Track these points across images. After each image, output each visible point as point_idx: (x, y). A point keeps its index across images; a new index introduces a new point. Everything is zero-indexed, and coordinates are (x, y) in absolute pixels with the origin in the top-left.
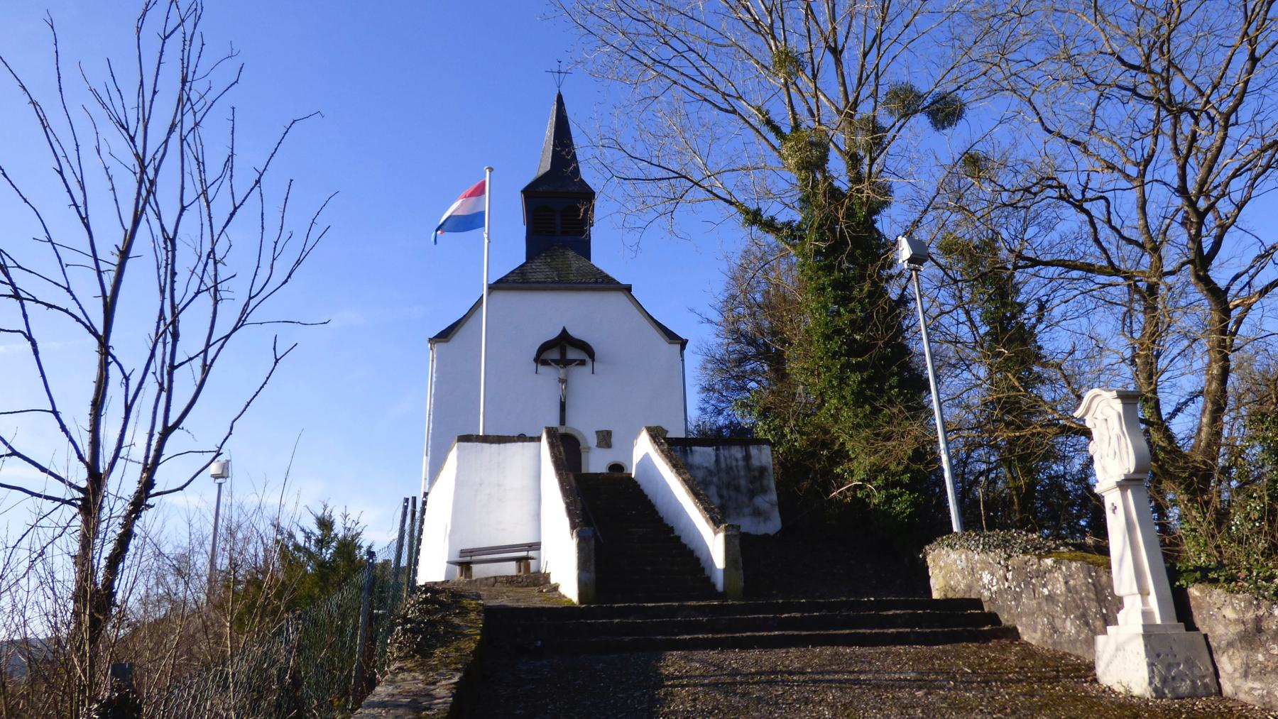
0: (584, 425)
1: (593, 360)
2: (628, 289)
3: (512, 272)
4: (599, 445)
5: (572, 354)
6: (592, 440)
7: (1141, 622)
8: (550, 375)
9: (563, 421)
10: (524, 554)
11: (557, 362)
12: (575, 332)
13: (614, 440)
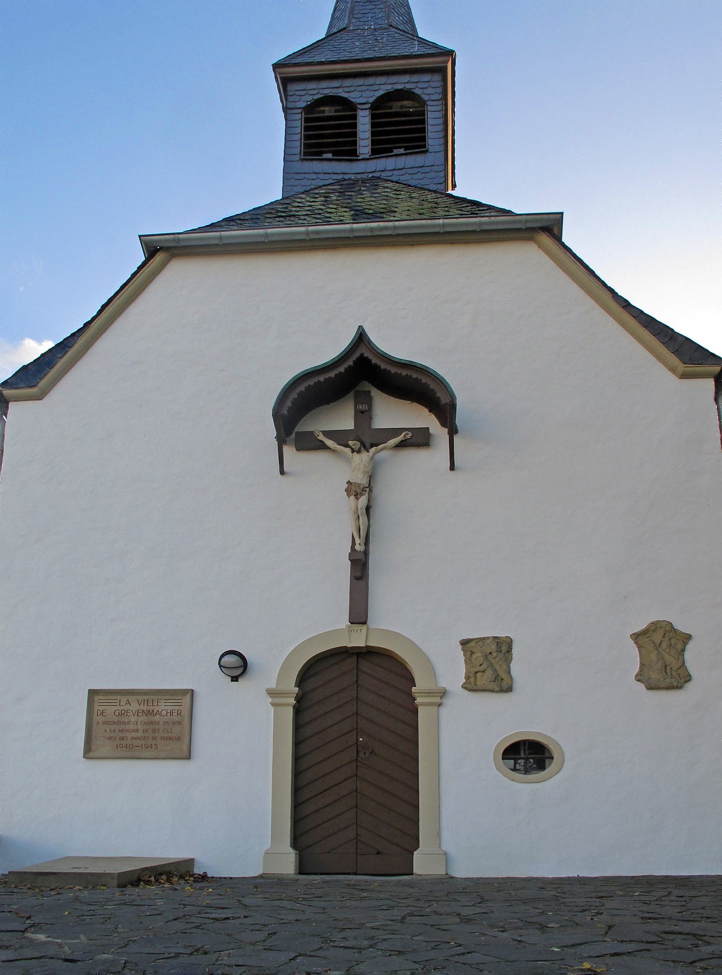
1: (453, 431)
2: (549, 227)
4: (471, 686)
5: (391, 414)
6: (451, 671)
7: (513, 665)
8: (326, 476)
9: (359, 615)
12: (394, 344)
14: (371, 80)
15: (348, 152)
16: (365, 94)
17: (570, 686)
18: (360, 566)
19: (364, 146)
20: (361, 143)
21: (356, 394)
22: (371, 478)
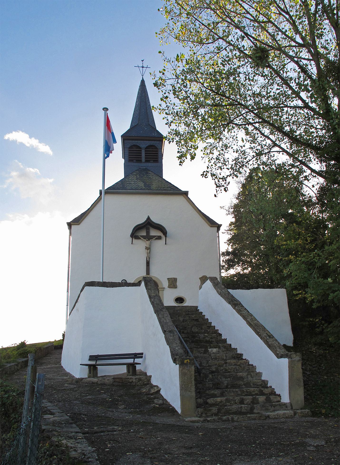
0: (160, 274)
1: (166, 237)
2: (186, 194)
3: (116, 184)
4: (169, 287)
5: (154, 233)
6: (165, 284)
8: (141, 245)
10: (131, 361)
11: (144, 237)
12: (155, 219)
13: (178, 284)
14: (145, 142)
15: (140, 161)
16: (143, 145)
17: (237, 267)
18: (148, 264)
19: (143, 159)
20: (143, 158)
21: (147, 230)
22: (150, 245)
